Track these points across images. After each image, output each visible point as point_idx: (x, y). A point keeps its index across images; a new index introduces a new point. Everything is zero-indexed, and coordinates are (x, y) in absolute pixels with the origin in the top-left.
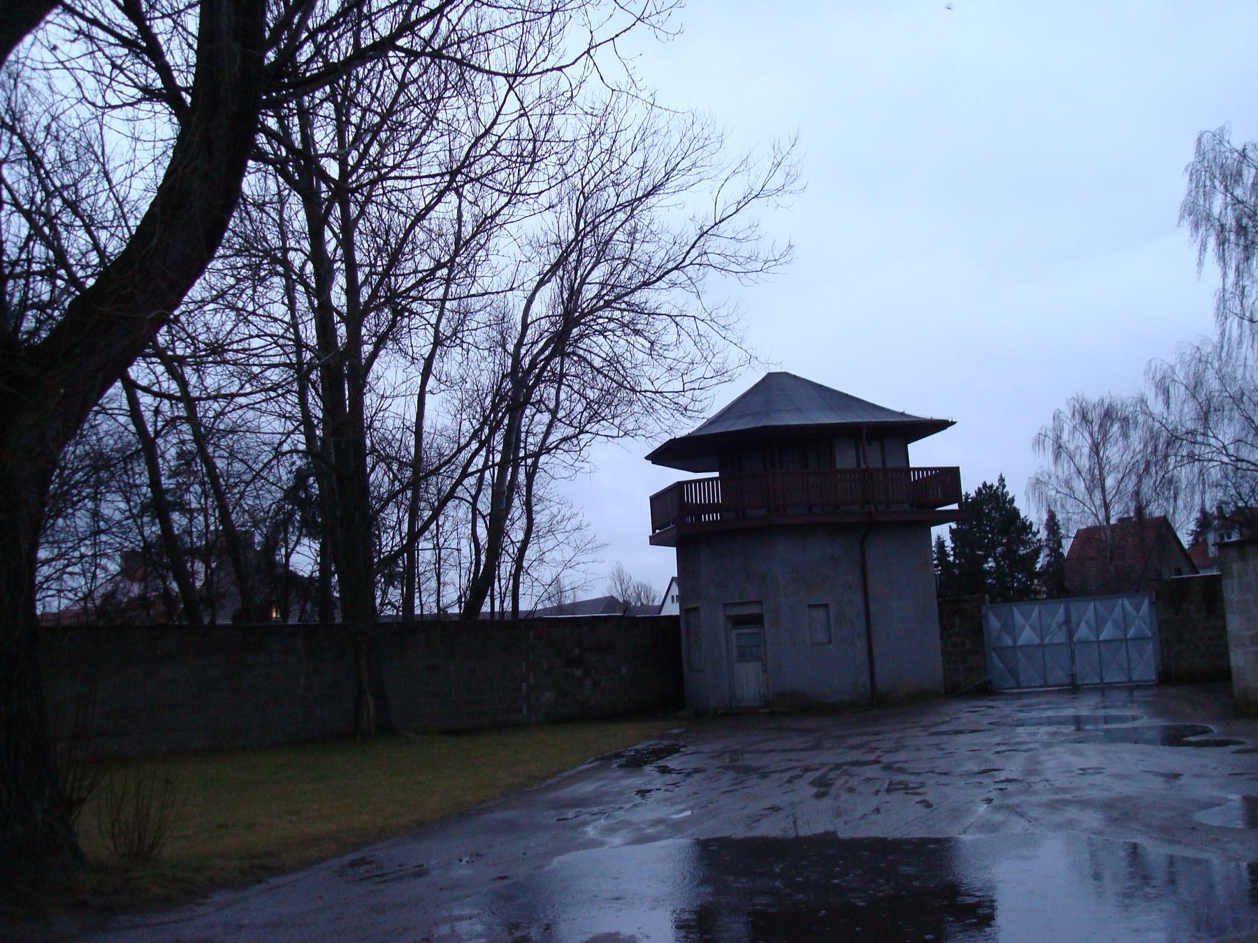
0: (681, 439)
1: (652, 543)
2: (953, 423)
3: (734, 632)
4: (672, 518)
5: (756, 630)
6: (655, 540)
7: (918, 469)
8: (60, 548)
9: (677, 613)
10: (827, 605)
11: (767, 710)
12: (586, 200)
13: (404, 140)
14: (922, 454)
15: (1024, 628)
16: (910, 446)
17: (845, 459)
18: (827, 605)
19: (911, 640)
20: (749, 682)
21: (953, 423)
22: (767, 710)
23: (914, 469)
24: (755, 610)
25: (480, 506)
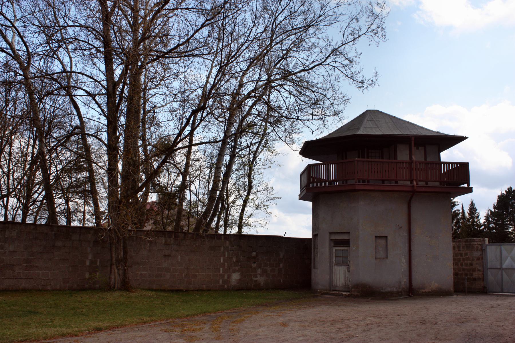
0: (317, 141)
1: (300, 199)
2: (466, 138)
3: (334, 249)
4: (312, 188)
5: (346, 248)
6: (302, 198)
7: (447, 163)
8: (80, 211)
9: (308, 234)
10: (386, 237)
11: (347, 294)
12: (277, 26)
13: (292, 89)
14: (447, 156)
15: (507, 258)
16: (441, 153)
17: (403, 155)
18: (386, 237)
19: (437, 262)
20: (340, 276)
21: (466, 138)
22: (347, 294)
23: (444, 163)
24: (345, 237)
25: (144, 77)
